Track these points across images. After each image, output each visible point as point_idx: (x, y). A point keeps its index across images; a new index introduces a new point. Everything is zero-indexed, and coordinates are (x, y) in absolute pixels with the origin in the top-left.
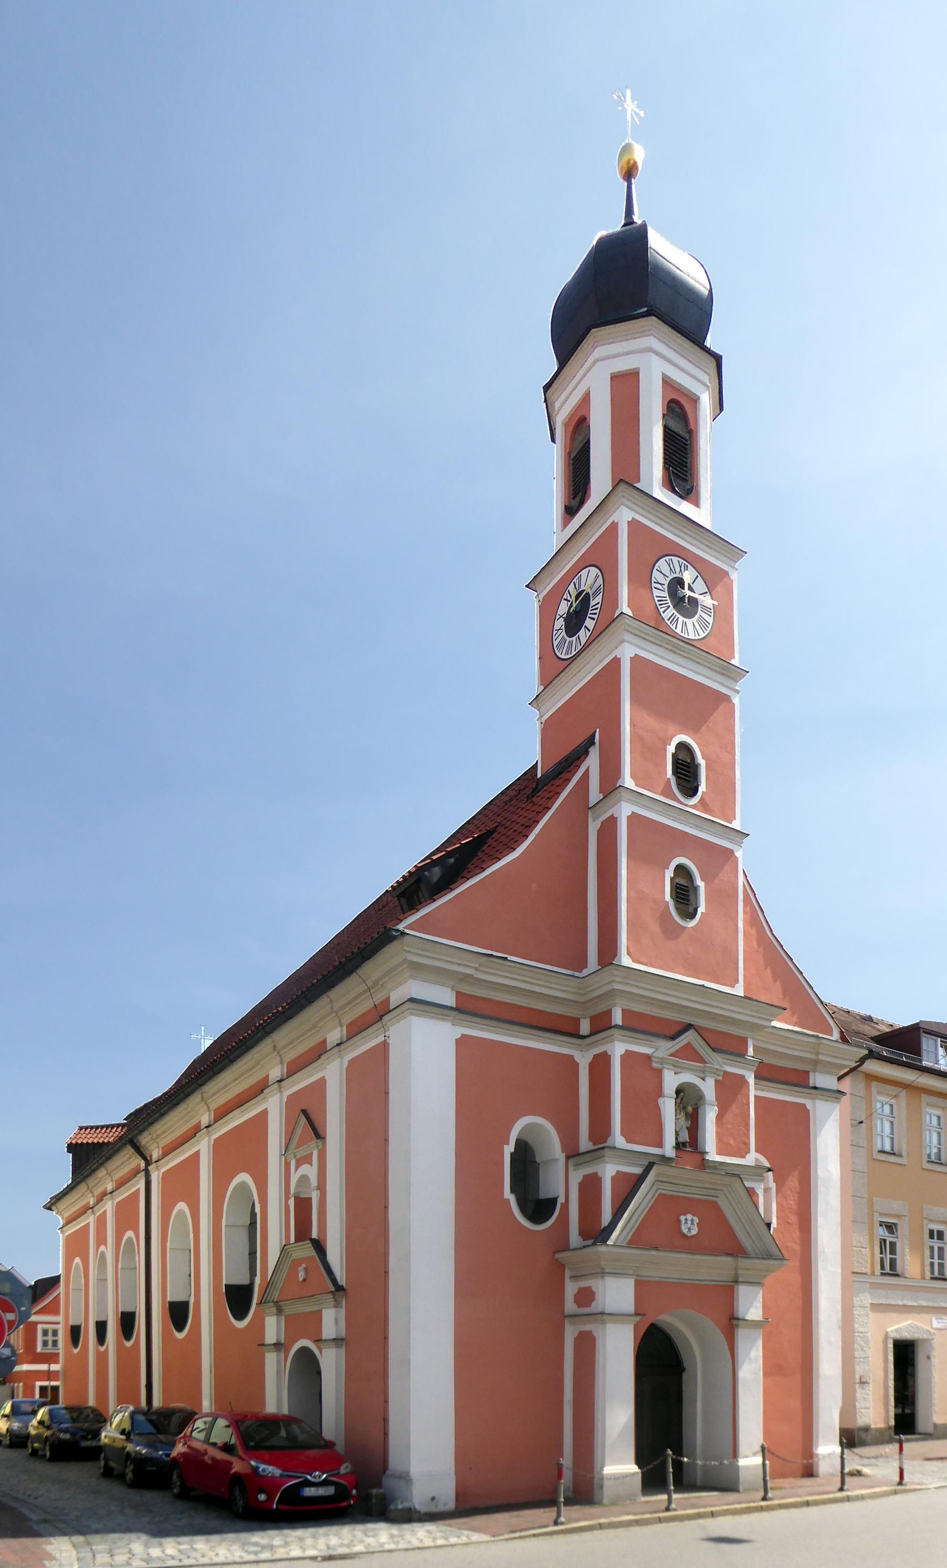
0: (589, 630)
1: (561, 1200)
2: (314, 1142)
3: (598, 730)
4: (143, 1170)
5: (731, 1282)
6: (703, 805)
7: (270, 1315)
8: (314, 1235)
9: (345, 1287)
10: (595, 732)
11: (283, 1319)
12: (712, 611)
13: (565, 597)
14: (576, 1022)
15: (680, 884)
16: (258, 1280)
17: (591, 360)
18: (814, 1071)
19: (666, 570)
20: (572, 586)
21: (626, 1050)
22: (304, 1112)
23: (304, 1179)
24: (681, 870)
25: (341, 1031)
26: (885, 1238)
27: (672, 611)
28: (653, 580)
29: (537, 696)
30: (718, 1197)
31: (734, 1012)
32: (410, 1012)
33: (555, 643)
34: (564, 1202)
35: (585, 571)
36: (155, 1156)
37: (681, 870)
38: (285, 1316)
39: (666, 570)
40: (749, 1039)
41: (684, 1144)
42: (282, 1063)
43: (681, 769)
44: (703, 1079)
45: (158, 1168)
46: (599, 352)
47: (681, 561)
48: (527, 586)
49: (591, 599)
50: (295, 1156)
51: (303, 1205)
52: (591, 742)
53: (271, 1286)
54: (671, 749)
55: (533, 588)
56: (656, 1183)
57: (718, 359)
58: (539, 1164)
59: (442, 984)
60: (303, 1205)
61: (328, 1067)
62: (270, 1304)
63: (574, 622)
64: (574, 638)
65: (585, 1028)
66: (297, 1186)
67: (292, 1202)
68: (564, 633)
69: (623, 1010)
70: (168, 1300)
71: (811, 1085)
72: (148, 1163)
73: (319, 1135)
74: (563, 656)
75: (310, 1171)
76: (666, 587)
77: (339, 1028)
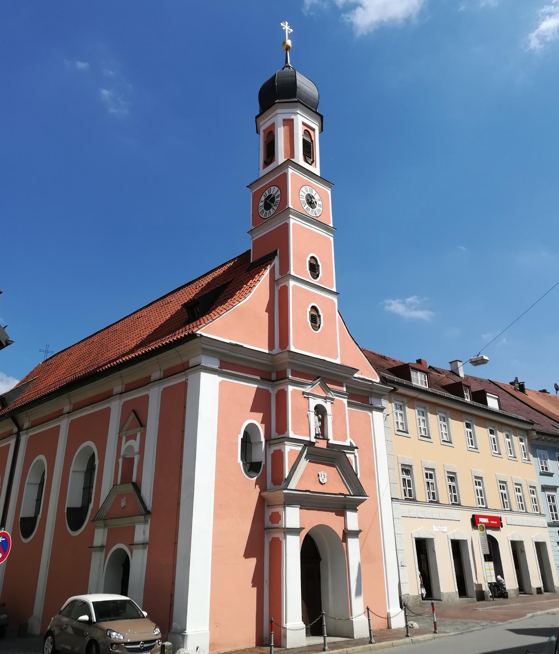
0: (275, 210)
1: (263, 463)
2: (139, 428)
3: (278, 249)
4: (16, 433)
5: (342, 509)
6: (321, 281)
7: (99, 527)
8: (134, 479)
9: (151, 512)
10: (277, 250)
11: (107, 530)
12: (322, 206)
13: (264, 194)
14: (270, 374)
15: (313, 314)
16: (91, 506)
17: (275, 113)
18: (371, 397)
19: (305, 191)
20: (267, 192)
21: (293, 389)
22: (134, 411)
23: (131, 448)
24: (313, 308)
25: (160, 373)
26: (405, 478)
27: (307, 206)
28: (300, 195)
29: (251, 230)
30: (334, 462)
31: (338, 371)
32: (201, 370)
33: (259, 211)
34: (264, 464)
35: (272, 188)
36: (26, 426)
37: (313, 308)
38: (108, 528)
39: (305, 191)
40: (344, 383)
41: (318, 435)
42: (122, 384)
43: (312, 267)
44: (326, 402)
45: (27, 433)
46: (279, 111)
47: (310, 187)
48: (247, 187)
49: (275, 199)
50: (126, 435)
51: (128, 463)
52: (275, 253)
53: (102, 510)
54: (308, 259)
55: (250, 188)
56: (308, 455)
57: (322, 117)
58: (252, 443)
59: (215, 357)
60: (128, 463)
61: (151, 390)
62: (101, 521)
63: (267, 206)
64: (268, 211)
65: (274, 377)
66: (125, 451)
67: (121, 461)
68: (263, 208)
69: (291, 370)
70: (20, 516)
71: (370, 403)
72: (20, 429)
73: (142, 424)
74: (263, 217)
75: (135, 444)
76: (305, 197)
77: (160, 371)
